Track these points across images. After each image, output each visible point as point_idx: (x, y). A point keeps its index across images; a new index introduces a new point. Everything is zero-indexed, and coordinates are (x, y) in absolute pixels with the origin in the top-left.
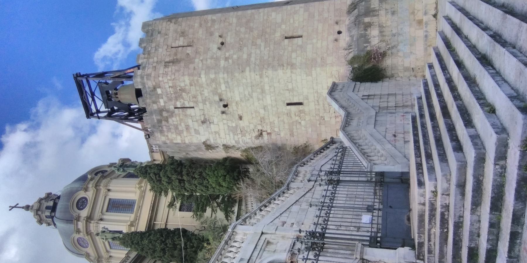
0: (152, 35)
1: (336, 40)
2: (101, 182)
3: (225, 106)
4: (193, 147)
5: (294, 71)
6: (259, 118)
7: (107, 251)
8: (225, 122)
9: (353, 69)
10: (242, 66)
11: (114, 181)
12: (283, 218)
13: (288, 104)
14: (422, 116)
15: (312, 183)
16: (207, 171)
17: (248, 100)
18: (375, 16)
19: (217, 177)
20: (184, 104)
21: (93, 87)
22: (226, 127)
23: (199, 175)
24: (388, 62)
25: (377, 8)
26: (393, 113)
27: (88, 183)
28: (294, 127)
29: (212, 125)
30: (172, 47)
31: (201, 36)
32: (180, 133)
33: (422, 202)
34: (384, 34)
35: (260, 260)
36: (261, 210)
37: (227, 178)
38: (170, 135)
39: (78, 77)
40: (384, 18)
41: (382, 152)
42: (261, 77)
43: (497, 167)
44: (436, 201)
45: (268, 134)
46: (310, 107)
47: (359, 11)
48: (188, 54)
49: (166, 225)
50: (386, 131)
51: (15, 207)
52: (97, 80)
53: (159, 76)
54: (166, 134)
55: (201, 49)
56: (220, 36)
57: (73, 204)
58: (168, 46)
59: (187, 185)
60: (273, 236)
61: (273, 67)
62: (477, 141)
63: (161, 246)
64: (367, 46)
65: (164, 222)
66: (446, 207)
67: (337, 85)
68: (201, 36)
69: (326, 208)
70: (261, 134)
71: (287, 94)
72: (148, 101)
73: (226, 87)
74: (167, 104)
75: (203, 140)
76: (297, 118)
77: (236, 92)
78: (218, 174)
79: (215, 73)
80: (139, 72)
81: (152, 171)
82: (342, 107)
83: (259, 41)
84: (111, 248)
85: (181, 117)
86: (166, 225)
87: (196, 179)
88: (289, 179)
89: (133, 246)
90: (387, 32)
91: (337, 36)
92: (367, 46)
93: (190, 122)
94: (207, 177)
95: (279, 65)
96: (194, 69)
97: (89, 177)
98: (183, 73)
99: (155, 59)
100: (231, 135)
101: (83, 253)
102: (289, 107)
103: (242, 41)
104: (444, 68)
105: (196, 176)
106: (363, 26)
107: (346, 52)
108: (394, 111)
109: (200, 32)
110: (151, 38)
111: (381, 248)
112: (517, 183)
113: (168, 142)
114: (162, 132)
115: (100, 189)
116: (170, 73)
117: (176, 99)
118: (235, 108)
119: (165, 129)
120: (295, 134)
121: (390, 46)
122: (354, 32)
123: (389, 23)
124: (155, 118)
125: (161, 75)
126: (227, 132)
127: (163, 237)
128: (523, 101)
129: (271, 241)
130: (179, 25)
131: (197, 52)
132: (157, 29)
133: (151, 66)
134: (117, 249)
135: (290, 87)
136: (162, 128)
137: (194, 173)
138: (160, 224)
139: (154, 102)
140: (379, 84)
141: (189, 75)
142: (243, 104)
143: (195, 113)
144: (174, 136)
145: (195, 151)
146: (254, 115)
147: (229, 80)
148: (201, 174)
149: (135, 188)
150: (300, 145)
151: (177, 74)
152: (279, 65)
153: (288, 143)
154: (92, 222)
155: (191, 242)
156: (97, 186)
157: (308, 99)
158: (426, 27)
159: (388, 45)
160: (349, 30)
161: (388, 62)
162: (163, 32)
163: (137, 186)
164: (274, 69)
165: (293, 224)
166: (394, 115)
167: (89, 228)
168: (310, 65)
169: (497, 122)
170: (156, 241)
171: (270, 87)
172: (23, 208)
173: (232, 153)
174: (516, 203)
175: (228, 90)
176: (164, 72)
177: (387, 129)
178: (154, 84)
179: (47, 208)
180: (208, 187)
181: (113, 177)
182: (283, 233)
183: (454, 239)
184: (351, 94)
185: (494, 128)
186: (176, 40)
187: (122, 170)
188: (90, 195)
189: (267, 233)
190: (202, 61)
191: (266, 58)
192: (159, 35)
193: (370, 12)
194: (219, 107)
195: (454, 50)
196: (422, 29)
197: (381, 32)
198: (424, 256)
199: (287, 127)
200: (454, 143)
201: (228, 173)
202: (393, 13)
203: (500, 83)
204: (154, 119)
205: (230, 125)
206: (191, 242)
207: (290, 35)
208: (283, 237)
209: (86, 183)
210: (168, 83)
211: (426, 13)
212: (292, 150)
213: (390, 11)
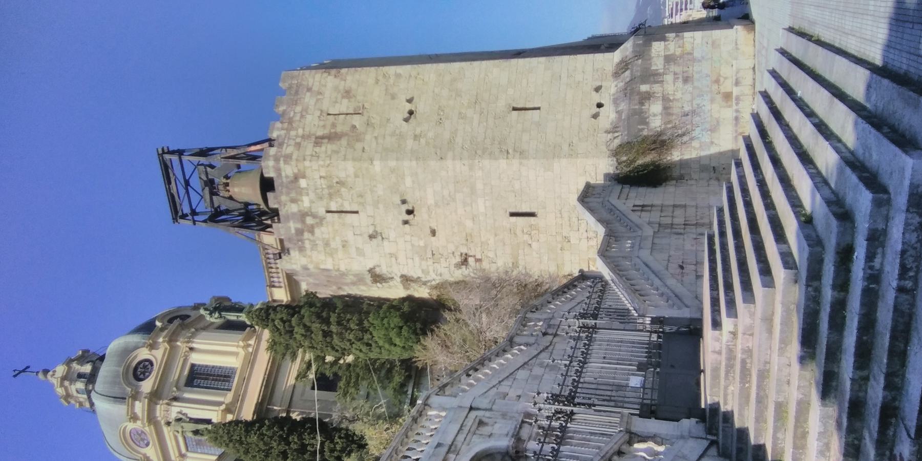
0: (297, 93)
3: (410, 212)
4: (351, 277)
5: (525, 162)
6: (464, 234)
8: (408, 238)
12: (503, 388)
13: (513, 214)
14: (723, 234)
15: (550, 338)
19: (386, 329)
20: (342, 205)
21: (189, 169)
23: (357, 325)
25: (661, 71)
26: (681, 234)
27: (157, 336)
28: (521, 252)
29: (386, 243)
30: (329, 114)
32: (332, 254)
33: (717, 349)
34: (670, 111)
36: (469, 375)
37: (405, 331)
40: (670, 86)
42: (471, 168)
43: (810, 289)
44: (735, 345)
47: (632, 72)
48: (354, 127)
50: (669, 260)
52: (196, 159)
53: (304, 160)
54: (308, 252)
56: (410, 101)
58: (322, 111)
59: (336, 340)
60: (488, 414)
61: (490, 154)
62: (789, 259)
66: (748, 352)
70: (465, 262)
72: (284, 198)
73: (413, 182)
76: (526, 237)
77: (430, 191)
78: (389, 323)
80: (273, 151)
81: (279, 316)
84: (187, 450)
87: (352, 330)
89: (231, 445)
90: (676, 110)
91: (595, 110)
93: (350, 236)
97: (158, 324)
98: (345, 156)
99: (300, 131)
100: (417, 259)
102: (514, 219)
103: (443, 111)
104: (756, 167)
105: (353, 326)
106: (637, 97)
107: (610, 136)
108: (682, 231)
112: (831, 307)
113: (311, 266)
114: (302, 249)
116: (323, 155)
119: (307, 245)
122: (623, 106)
123: (678, 95)
124: (293, 226)
125: (308, 158)
127: (283, 430)
128: (841, 207)
129: (485, 420)
130: (342, 79)
133: (292, 142)
136: (303, 243)
137: (348, 321)
139: (294, 201)
140: (660, 190)
143: (362, 222)
144: (322, 257)
145: (354, 284)
148: (360, 323)
155: (332, 441)
157: (545, 208)
158: (737, 104)
160: (616, 102)
162: (315, 88)
164: (492, 156)
168: (552, 152)
169: (814, 235)
170: (271, 438)
171: (485, 184)
173: (414, 289)
174: (829, 333)
177: (670, 256)
178: (296, 171)
180: (371, 345)
181: (199, 326)
183: (757, 394)
185: (807, 240)
186: (336, 102)
189: (478, 409)
190: (376, 138)
192: (308, 94)
193: (650, 76)
195: (771, 142)
196: (730, 106)
197: (665, 108)
198: (717, 430)
200: (761, 265)
201: (406, 323)
202: (686, 80)
203: (819, 185)
204: (290, 227)
205: (417, 244)
206: (332, 441)
211: (737, 83)
213: (680, 76)
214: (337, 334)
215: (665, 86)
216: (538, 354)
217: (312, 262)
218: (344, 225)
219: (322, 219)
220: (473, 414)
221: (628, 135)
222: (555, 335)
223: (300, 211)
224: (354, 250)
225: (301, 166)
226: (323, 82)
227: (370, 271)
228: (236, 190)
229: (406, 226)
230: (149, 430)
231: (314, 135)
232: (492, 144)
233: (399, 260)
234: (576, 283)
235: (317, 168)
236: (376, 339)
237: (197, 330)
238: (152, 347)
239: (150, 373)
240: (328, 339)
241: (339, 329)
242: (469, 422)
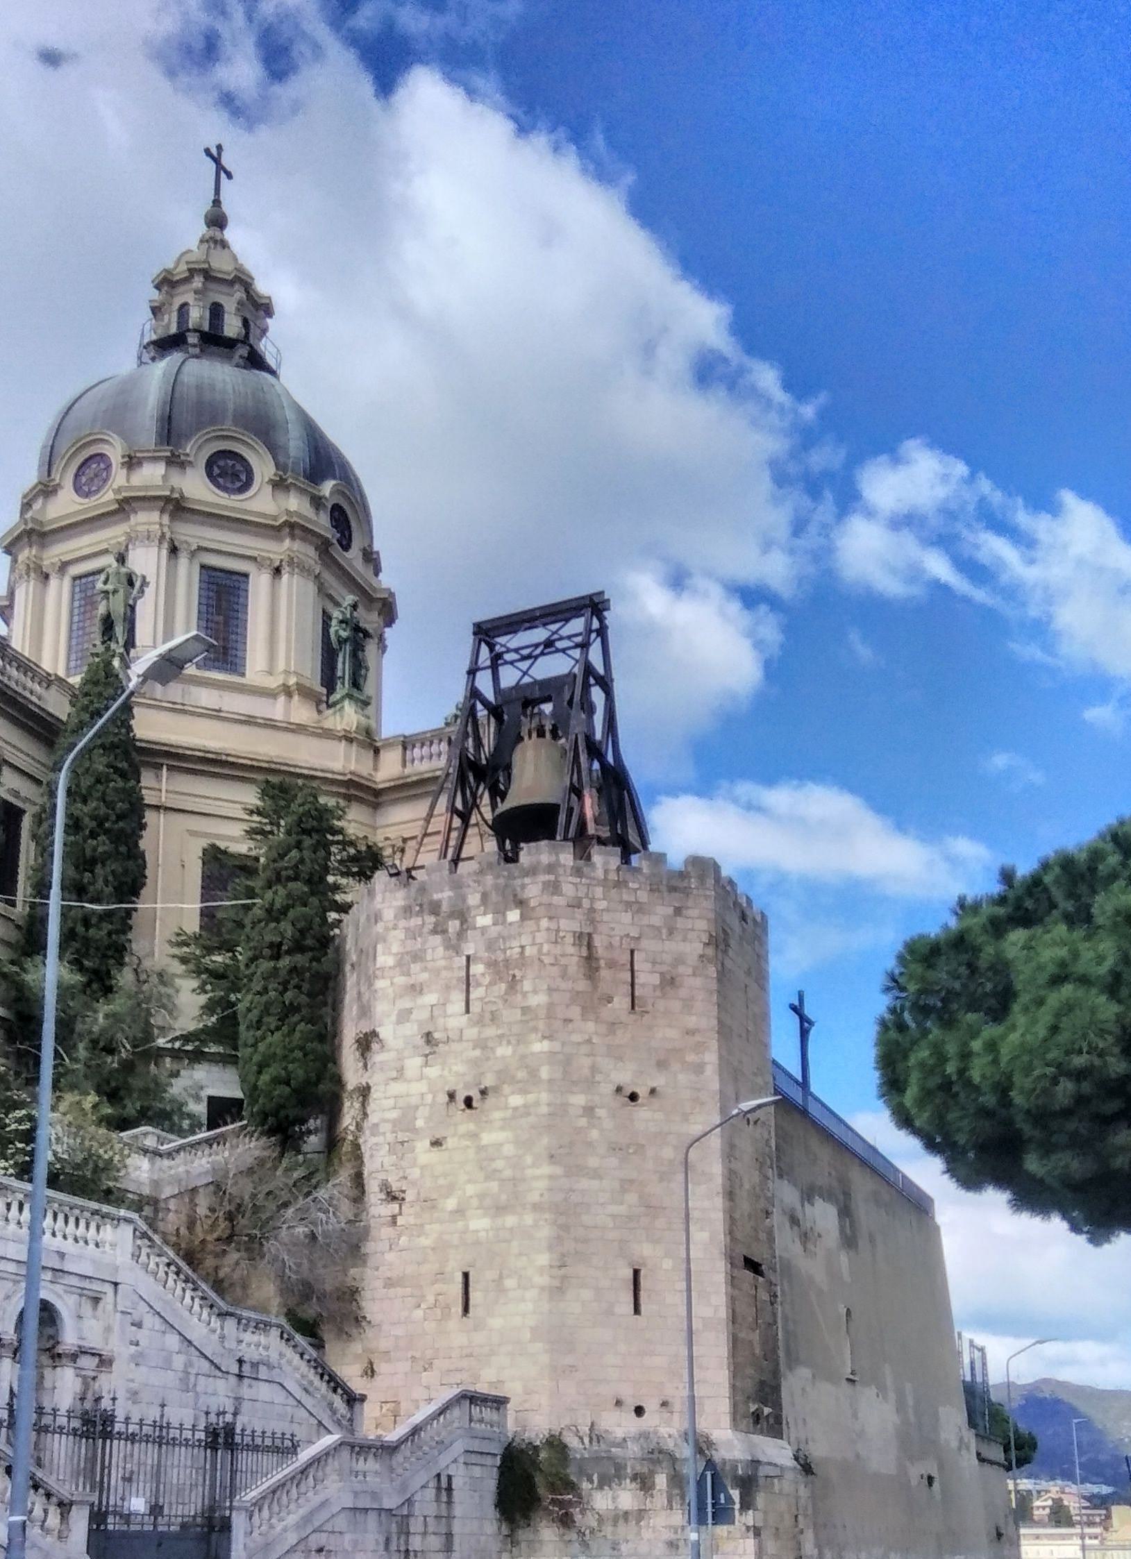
0: (673, 889)
1: (619, 1403)
2: (303, 539)
3: (468, 1102)
6: (434, 1196)
7: (64, 566)
9: (536, 1448)
10: (567, 1156)
11: (311, 588)
12: (150, 1321)
13: (466, 1276)
16: (302, 1026)
17: (481, 1168)
18: (670, 1502)
19: (285, 1057)
20: (479, 985)
22: (414, 1101)
23: (291, 1004)
24: (548, 1533)
29: (419, 1061)
30: (632, 952)
31: (660, 1035)
34: (621, 1522)
35: (61, 1292)
38: (399, 934)
39: (595, 606)
41: (279, 1528)
42: (536, 1207)
45: (394, 1217)
46: (457, 1332)
48: (610, 1000)
49: (157, 808)
50: (333, 1532)
51: (220, 168)
53: (550, 918)
54: (402, 923)
55: (622, 1037)
56: (653, 1091)
58: (638, 938)
59: (265, 965)
60: (110, 1307)
63: (87, 820)
64: (592, 1482)
65: (164, 799)
67: (498, 1409)
68: (660, 1035)
69: (157, 1434)
70: (392, 1197)
71: (491, 1275)
73: (515, 1109)
74: (478, 932)
75: (385, 1032)
76: (431, 1299)
79: (550, 1081)
81: (306, 854)
83: (632, 1198)
84: (75, 579)
86: (157, 808)
87: (282, 994)
88: (245, 1314)
91: (631, 1403)
92: (592, 1482)
93: (430, 998)
94: (285, 1028)
95: (563, 1255)
100: (394, 1115)
101: (56, 476)
102: (459, 1278)
103: (635, 1153)
105: (289, 995)
106: (645, 1470)
108: (393, 1547)
109: (672, 1033)
110: (664, 888)
113: (380, 928)
115: (281, 540)
116: (558, 950)
117: (491, 964)
118: (463, 1129)
120: (392, 1292)
122: (634, 1449)
123: (647, 1534)
124: (444, 896)
125: (553, 926)
126: (401, 1103)
129: (101, 1305)
130: (695, 968)
131: (613, 1026)
132: (690, 903)
134: (73, 600)
135: (510, 1283)
137: (298, 987)
138: (157, 786)
139: (485, 897)
141: (551, 1006)
142: (471, 1153)
144: (395, 948)
146: (441, 1181)
147: (532, 1119)
148: (293, 1009)
149: (287, 672)
150: (363, 1304)
151: (555, 971)
152: (563, 1255)
153: (369, 1272)
154: (166, 519)
156: (293, 528)
160: (644, 1436)
161: (548, 1533)
162: (680, 923)
163: (292, 681)
165: (137, 1345)
166: (382, 1547)
167: (144, 509)
168: (559, 1339)
170: (103, 799)
171: (511, 1229)
172: (217, 202)
175: (509, 1113)
176: (561, 934)
178: (532, 903)
179: (216, 312)
182: (116, 1328)
184: (459, 1447)
186: (654, 963)
187: (344, 634)
188: (261, 501)
189: (116, 1292)
190: (589, 1041)
191: (586, 1219)
192: (670, 910)
194: (467, 1086)
199: (410, 1270)
201: (294, 1090)
204: (442, 891)
207: (643, 1283)
208: (108, 1329)
209: (302, 482)
210: (534, 944)
212: (349, 1282)
214: (275, 968)
215: (664, 1513)
216: (206, 1358)
217: (387, 929)
218: (448, 988)
219: (457, 951)
220: (109, 1289)
222: (240, 1377)
223: (468, 908)
225: (541, 911)
226: (691, 935)
227: (374, 1034)
228: (530, 754)
229: (447, 1098)
231: (595, 928)
232: (576, 1240)
233: (393, 1084)
234: (339, 1391)
235: (538, 941)
236: (269, 1039)
237: (317, 577)
238: (279, 485)
239: (224, 489)
242: (96, 1286)
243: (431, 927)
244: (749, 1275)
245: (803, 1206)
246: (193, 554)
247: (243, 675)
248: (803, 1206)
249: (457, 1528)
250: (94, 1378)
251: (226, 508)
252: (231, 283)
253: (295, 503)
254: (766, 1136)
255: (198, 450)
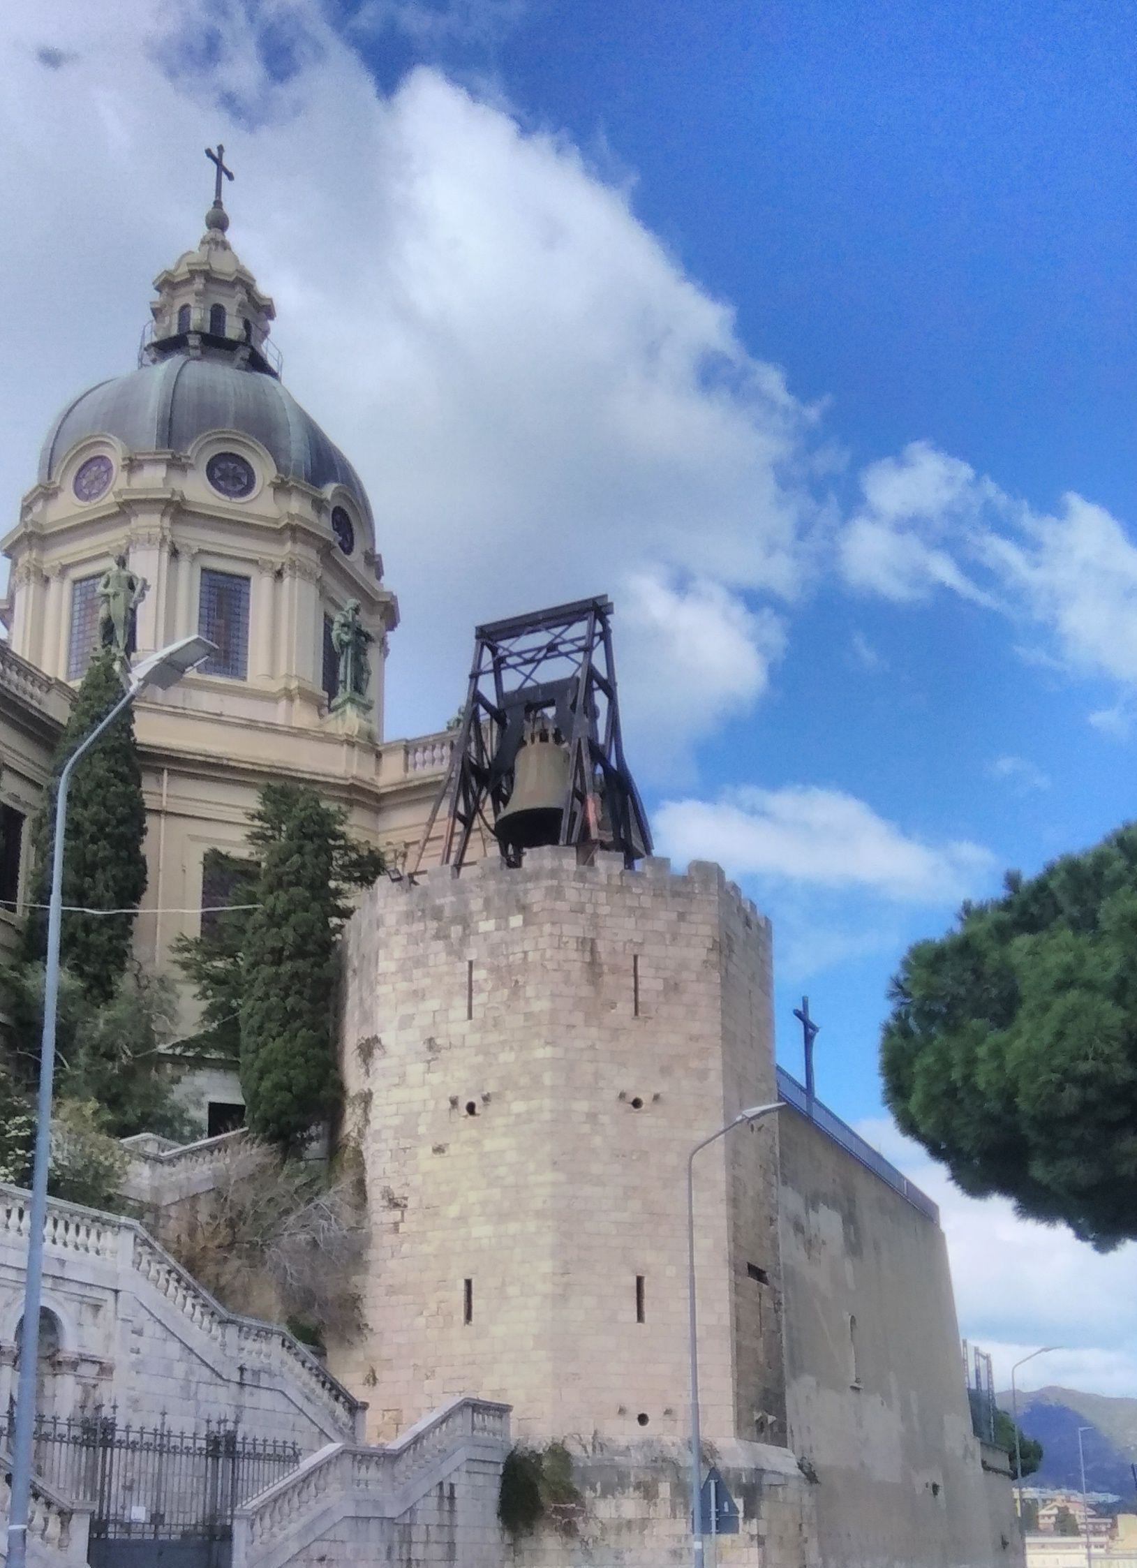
0: (676, 894)
1: (622, 1411)
2: (305, 543)
3: (471, 1108)
7: (64, 569)
9: (539, 1457)
11: (313, 592)
12: (151, 1329)
13: (468, 1283)
18: (673, 1510)
19: (287, 1063)
20: (481, 991)
23: (293, 1009)
27: (304, 494)
29: (421, 1067)
30: (636, 958)
32: (404, 971)
34: (624, 1531)
35: (62, 1300)
38: (402, 939)
39: (597, 610)
42: (539, 1214)
45: (396, 1224)
48: (613, 1005)
49: (158, 812)
51: (221, 168)
53: (553, 923)
54: (405, 929)
56: (656, 1098)
57: (228, 440)
58: (642, 944)
59: (267, 971)
60: (111, 1315)
63: (87, 824)
64: (595, 1491)
65: (165, 804)
67: (501, 1417)
70: (394, 1204)
73: (518, 1115)
75: (385, 1038)
76: (433, 1306)
81: (308, 858)
82: (418, 1439)
84: (75, 582)
85: (447, 979)
86: (158, 812)
87: (283, 999)
88: (247, 1321)
92: (595, 1491)
93: (433, 1004)
96: (571, 1027)
97: (329, 490)
100: (396, 1121)
101: (57, 479)
105: (290, 1001)
106: (649, 1478)
108: (395, 1556)
111: (90, 1539)
113: (382, 933)
115: (282, 543)
121: (591, 1546)
122: (637, 1458)
124: (447, 901)
125: (556, 931)
129: (102, 1312)
131: (616, 1032)
135: (512, 1290)
137: (300, 993)
138: (158, 791)
139: (487, 902)
140: (493, 1521)
143: (457, 1024)
144: (397, 954)
146: (444, 1188)
148: (294, 1015)
149: (288, 676)
153: (371, 1280)
154: (167, 522)
156: (294, 531)
159: (595, 1541)
160: (648, 1444)
162: (684, 928)
163: (294, 685)
165: (138, 1352)
166: (384, 1556)
167: (144, 512)
172: (218, 204)
176: (564, 939)
178: (535, 909)
179: (218, 314)
184: (461, 1456)
186: (658, 968)
187: (346, 638)
188: (262, 503)
189: (116, 1300)
190: (592, 1047)
192: (674, 916)
208: (109, 1337)
209: (305, 486)
212: (352, 1290)
214: (277, 974)
216: (207, 1365)
217: (389, 934)
220: (109, 1296)
221: (586, 1467)
222: (241, 1385)
223: (471, 913)
224: (410, 1012)
229: (449, 1105)
230: (107, 500)
234: (341, 1399)
235: (541, 946)
237: (319, 580)
238: (280, 487)
240: (268, 957)
241: (285, 979)
242: (96, 1294)
243: (433, 932)
244: (753, 1282)
245: (807, 1213)
246: (194, 557)
247: (244, 679)
248: (807, 1213)
249: (459, 1536)
250: (95, 1386)
251: (227, 511)
252: (232, 285)
253: (297, 506)
254: (770, 1142)
255: (199, 453)
